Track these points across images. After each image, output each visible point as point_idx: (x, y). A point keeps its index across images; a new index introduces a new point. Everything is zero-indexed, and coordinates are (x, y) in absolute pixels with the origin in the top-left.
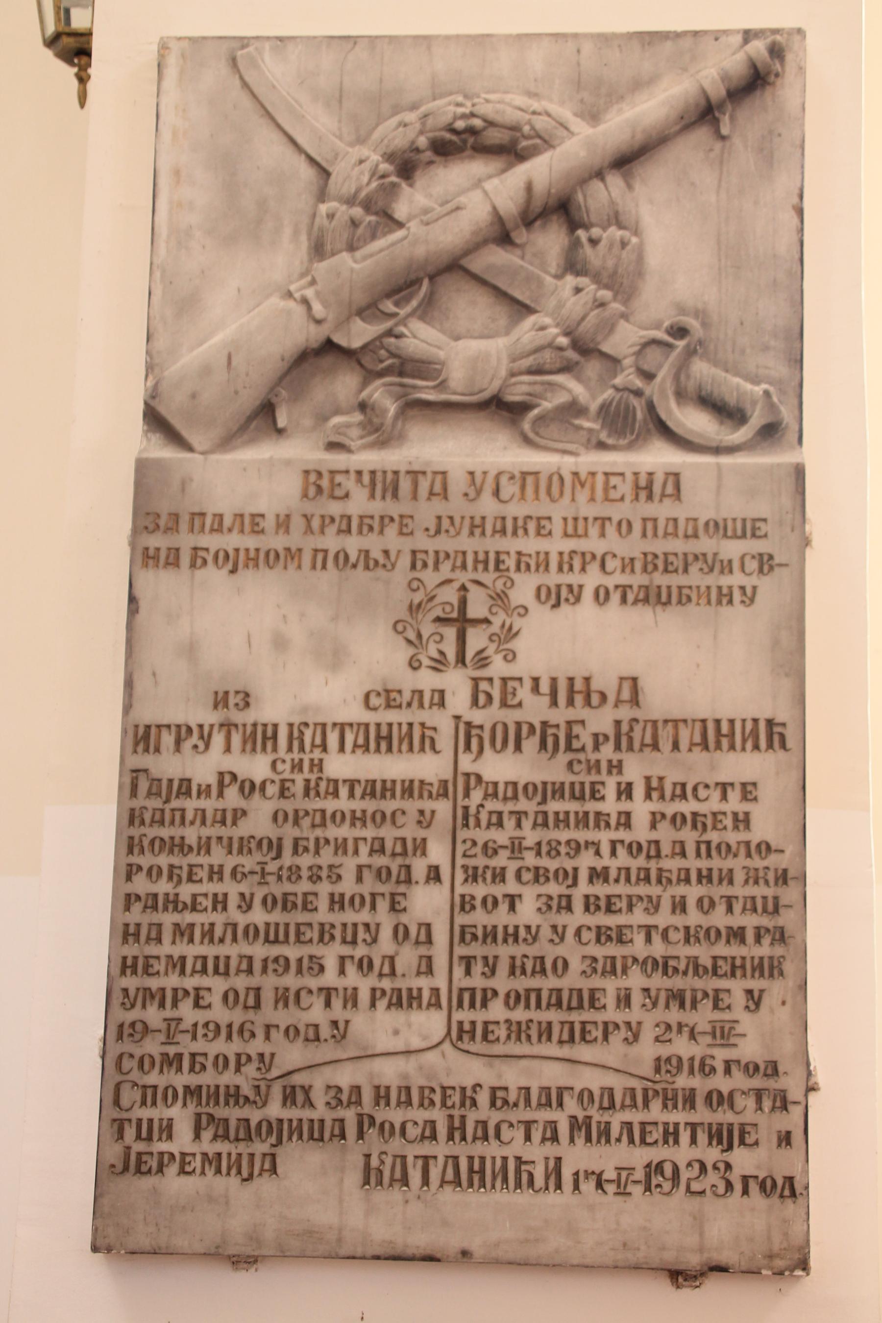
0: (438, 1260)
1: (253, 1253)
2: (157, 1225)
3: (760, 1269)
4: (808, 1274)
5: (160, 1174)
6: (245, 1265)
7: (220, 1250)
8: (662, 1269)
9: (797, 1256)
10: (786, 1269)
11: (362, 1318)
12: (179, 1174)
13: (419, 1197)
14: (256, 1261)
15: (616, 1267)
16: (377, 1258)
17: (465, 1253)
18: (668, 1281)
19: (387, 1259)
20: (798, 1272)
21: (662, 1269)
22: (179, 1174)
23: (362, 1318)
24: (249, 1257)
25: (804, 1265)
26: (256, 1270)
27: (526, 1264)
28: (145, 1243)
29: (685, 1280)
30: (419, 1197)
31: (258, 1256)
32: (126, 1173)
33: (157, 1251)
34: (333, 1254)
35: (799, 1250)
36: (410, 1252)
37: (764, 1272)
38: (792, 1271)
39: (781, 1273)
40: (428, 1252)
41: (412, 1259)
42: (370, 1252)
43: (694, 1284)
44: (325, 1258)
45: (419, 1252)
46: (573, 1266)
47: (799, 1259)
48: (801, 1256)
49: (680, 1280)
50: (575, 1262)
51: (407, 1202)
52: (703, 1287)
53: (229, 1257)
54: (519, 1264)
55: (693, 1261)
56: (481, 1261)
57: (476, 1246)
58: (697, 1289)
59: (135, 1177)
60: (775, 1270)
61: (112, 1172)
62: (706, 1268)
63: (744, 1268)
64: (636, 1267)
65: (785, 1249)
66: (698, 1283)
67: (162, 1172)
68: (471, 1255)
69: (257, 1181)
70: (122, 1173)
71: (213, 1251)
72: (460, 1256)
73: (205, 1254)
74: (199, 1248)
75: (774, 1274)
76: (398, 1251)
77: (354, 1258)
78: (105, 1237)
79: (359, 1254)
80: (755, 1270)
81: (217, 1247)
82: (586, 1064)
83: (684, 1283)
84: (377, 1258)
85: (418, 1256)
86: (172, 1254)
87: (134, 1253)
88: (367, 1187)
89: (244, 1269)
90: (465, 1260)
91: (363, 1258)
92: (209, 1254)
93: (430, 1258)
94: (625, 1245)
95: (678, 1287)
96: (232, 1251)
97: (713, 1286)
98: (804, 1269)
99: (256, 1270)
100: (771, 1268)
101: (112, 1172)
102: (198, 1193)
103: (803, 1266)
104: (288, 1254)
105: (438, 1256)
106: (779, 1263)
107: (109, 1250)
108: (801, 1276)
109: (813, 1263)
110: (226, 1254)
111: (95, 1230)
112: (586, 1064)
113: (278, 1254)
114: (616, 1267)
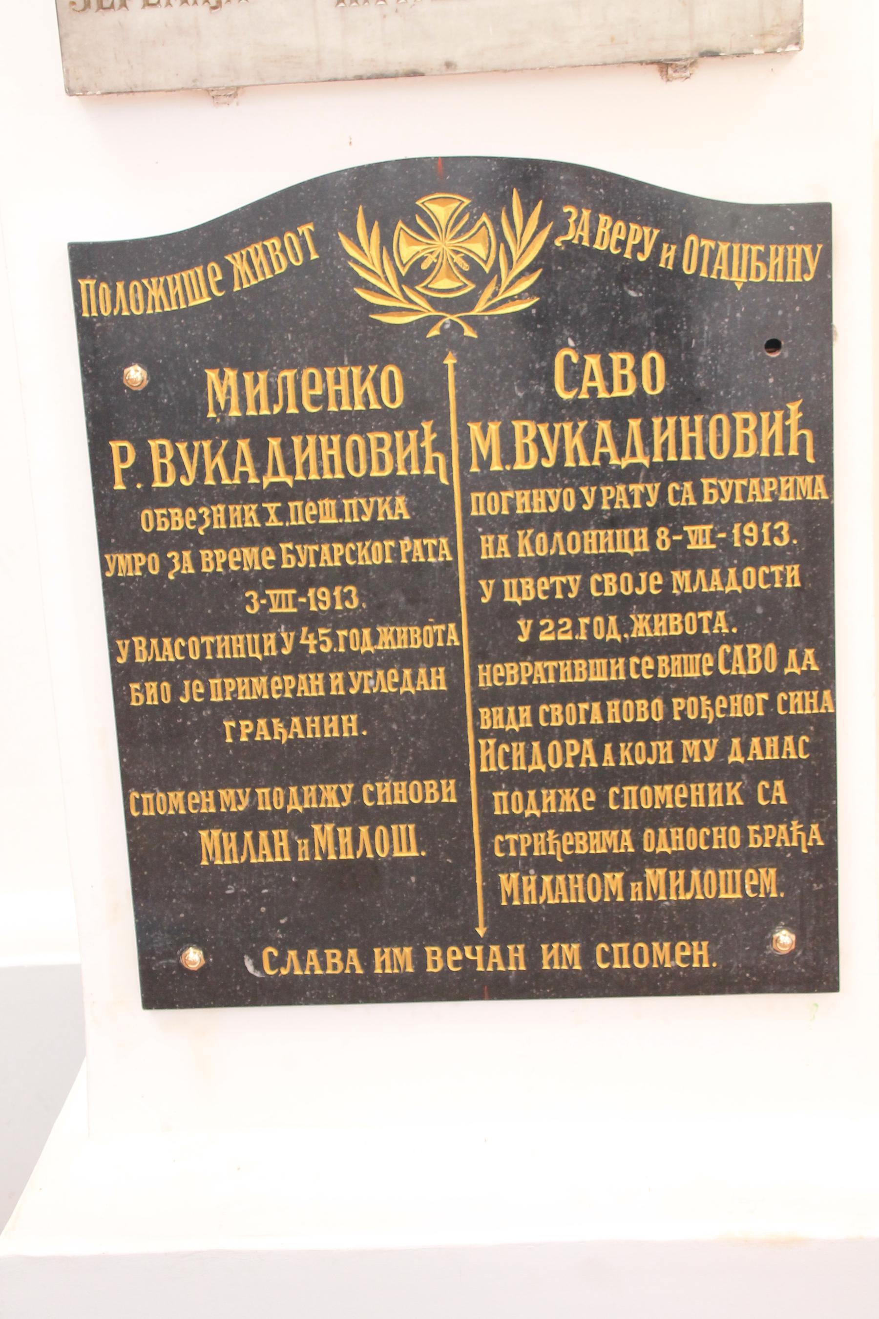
0: (422, 75)
1: (232, 84)
2: (129, 62)
3: (752, 49)
4: (801, 49)
5: (124, 8)
6: (226, 99)
7: (198, 84)
8: (652, 63)
9: (790, 31)
10: (779, 47)
11: (350, 143)
12: (144, 7)
13: (397, 11)
14: (235, 95)
15: (605, 64)
16: (360, 78)
17: (448, 65)
18: (657, 75)
19: (369, 78)
20: (791, 48)
21: (652, 63)
22: (144, 7)
23: (350, 143)
24: (228, 88)
25: (797, 39)
26: (238, 104)
27: (513, 70)
28: (121, 83)
29: (675, 71)
30: (397, 11)
31: (238, 88)
32: (87, 10)
33: (134, 90)
34: (315, 79)
35: (792, 25)
36: (392, 69)
37: (756, 52)
38: (785, 47)
39: (773, 52)
40: (412, 67)
41: (395, 76)
42: (351, 74)
43: (684, 75)
44: (305, 82)
45: (402, 68)
46: (560, 67)
47: (792, 33)
48: (794, 31)
49: (670, 71)
50: (563, 63)
51: (385, 17)
52: (692, 77)
53: (208, 91)
54: (505, 71)
55: (683, 49)
56: (466, 71)
57: (458, 56)
58: (688, 80)
59: (98, 14)
60: (768, 49)
61: (74, 10)
62: (696, 55)
63: (735, 51)
64: (624, 63)
65: (778, 25)
66: (688, 74)
67: (125, 6)
68: (456, 66)
69: (225, 8)
70: (84, 10)
71: (190, 84)
72: (444, 68)
73: (183, 89)
74: (176, 84)
75: (766, 52)
76: (380, 69)
77: (335, 80)
78: (77, 79)
79: (340, 76)
80: (748, 51)
81: (195, 81)
82: (139, 92)
83: (675, 75)
84: (360, 78)
85: (401, 72)
86: (150, 91)
87: (110, 93)
88: (342, 5)
89: (225, 103)
90: (449, 72)
91: (345, 79)
92: (187, 89)
93: (414, 74)
94: (612, 39)
95: (668, 80)
96: (209, 83)
97: (705, 73)
98: (797, 44)
99: (238, 104)
100: (764, 47)
101: (74, 10)
102: (166, 25)
103: (795, 41)
104: (267, 82)
105: (422, 70)
106: (771, 41)
107: (84, 92)
108: (795, 52)
109: (806, 36)
110: (205, 86)
111: (67, 72)
112: (139, 92)
113: (258, 83)
114: (605, 64)
